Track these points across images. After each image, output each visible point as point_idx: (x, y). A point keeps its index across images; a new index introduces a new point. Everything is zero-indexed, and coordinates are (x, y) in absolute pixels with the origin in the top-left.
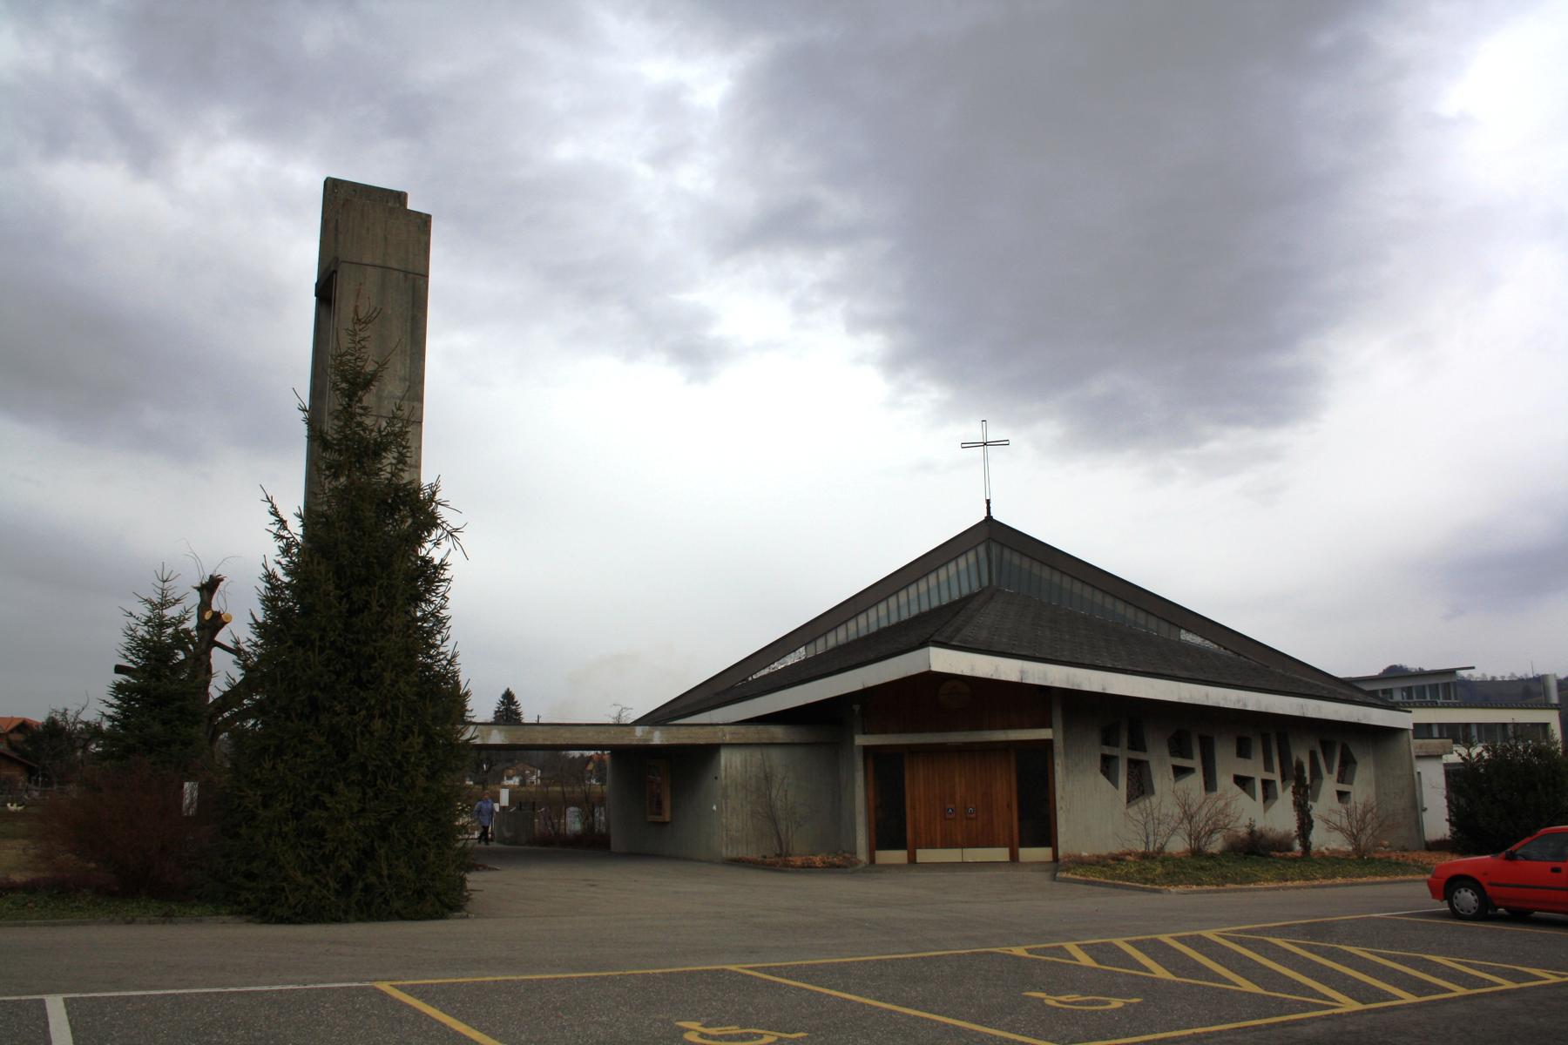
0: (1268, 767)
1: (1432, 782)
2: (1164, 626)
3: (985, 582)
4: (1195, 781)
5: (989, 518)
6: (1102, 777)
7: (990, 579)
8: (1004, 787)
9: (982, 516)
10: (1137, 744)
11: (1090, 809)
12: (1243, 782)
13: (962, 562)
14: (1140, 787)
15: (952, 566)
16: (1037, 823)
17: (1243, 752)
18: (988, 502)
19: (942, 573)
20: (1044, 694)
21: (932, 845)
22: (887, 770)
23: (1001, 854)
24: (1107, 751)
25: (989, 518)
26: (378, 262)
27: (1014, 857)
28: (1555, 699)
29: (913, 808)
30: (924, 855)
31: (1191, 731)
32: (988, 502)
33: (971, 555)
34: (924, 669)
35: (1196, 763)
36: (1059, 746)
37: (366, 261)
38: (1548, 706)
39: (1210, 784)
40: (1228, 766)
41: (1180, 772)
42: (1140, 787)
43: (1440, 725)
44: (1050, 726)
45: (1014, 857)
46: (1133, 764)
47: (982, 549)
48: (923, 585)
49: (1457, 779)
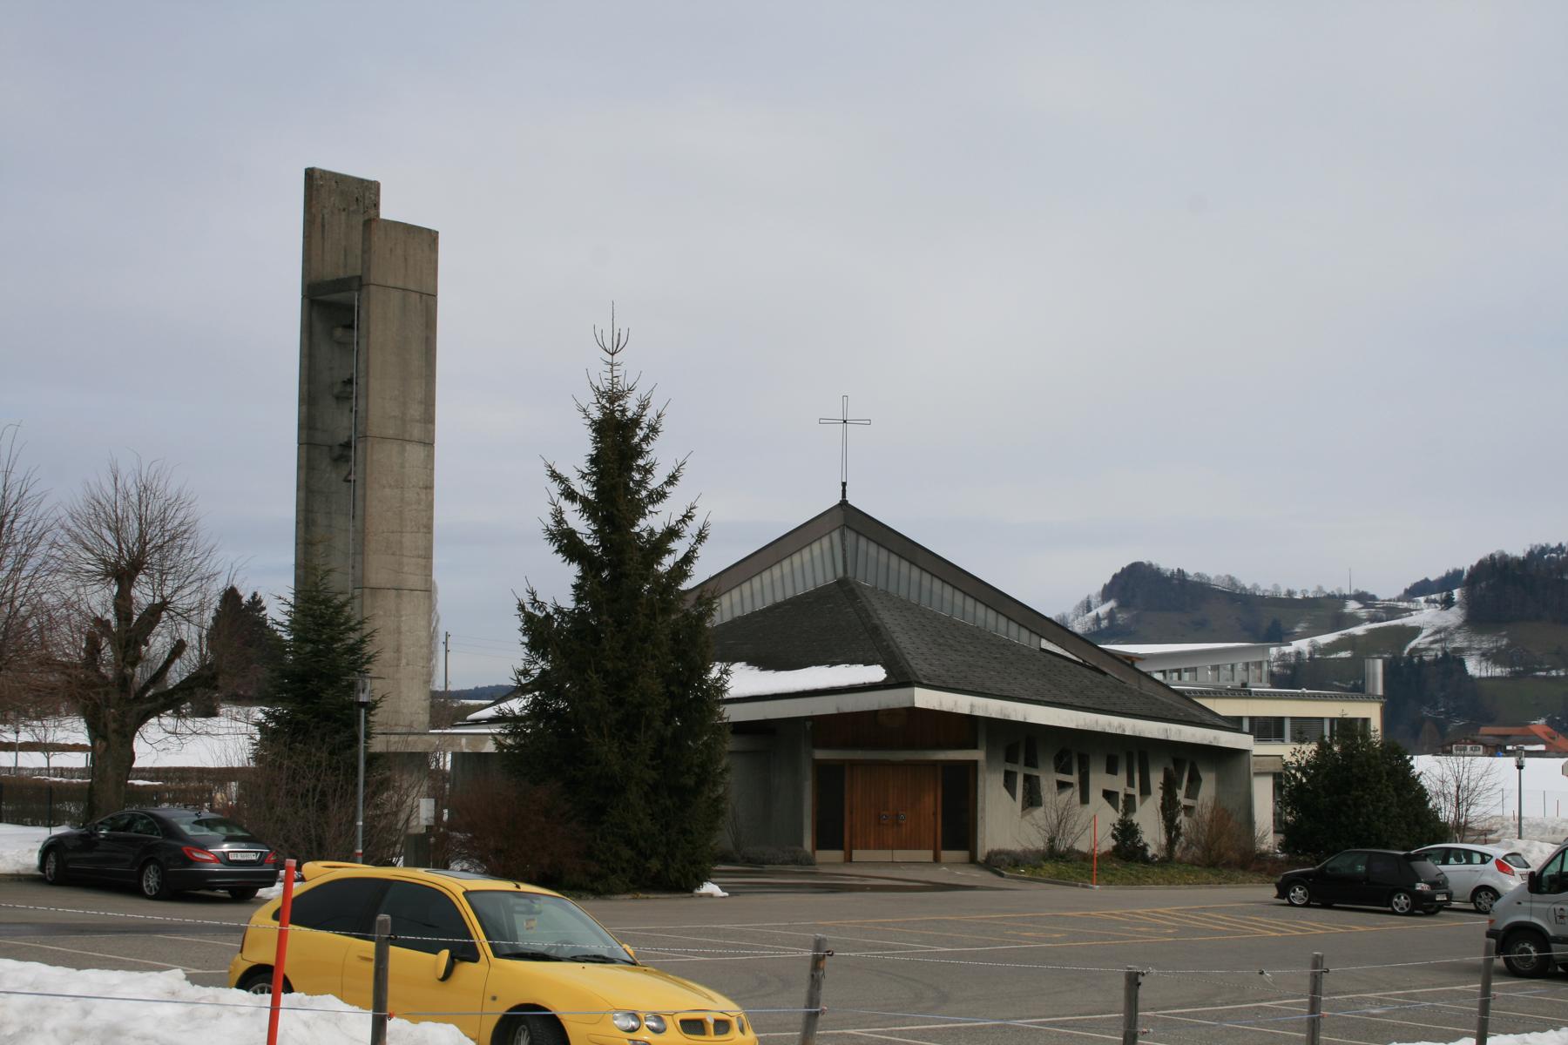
0: (1131, 783)
1: (1263, 798)
2: (1025, 634)
3: (840, 573)
4: (1074, 795)
5: (844, 503)
6: (1004, 791)
7: (845, 571)
8: (930, 802)
9: (837, 499)
10: (1031, 762)
11: (1003, 821)
12: (1109, 795)
13: (816, 547)
14: (1032, 799)
15: (806, 552)
16: (959, 829)
17: (1112, 769)
18: (844, 484)
19: (796, 558)
20: (971, 720)
21: (866, 847)
22: (830, 780)
23: (927, 855)
24: (1009, 767)
25: (844, 503)
26: (400, 284)
27: (937, 859)
28: (1380, 692)
29: (935, 814)
30: (858, 855)
31: (1074, 752)
32: (844, 484)
33: (826, 541)
34: (908, 705)
35: (1074, 778)
36: (982, 766)
37: (391, 283)
38: (1371, 698)
39: (1085, 799)
40: (1100, 780)
41: (1062, 786)
42: (1032, 799)
43: (1252, 719)
44: (975, 747)
45: (937, 859)
46: (1027, 778)
47: (836, 535)
48: (776, 570)
49: (1290, 791)
